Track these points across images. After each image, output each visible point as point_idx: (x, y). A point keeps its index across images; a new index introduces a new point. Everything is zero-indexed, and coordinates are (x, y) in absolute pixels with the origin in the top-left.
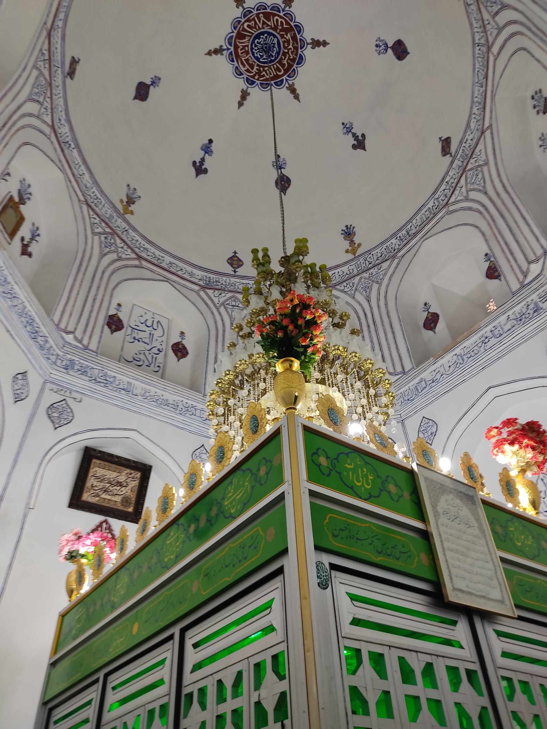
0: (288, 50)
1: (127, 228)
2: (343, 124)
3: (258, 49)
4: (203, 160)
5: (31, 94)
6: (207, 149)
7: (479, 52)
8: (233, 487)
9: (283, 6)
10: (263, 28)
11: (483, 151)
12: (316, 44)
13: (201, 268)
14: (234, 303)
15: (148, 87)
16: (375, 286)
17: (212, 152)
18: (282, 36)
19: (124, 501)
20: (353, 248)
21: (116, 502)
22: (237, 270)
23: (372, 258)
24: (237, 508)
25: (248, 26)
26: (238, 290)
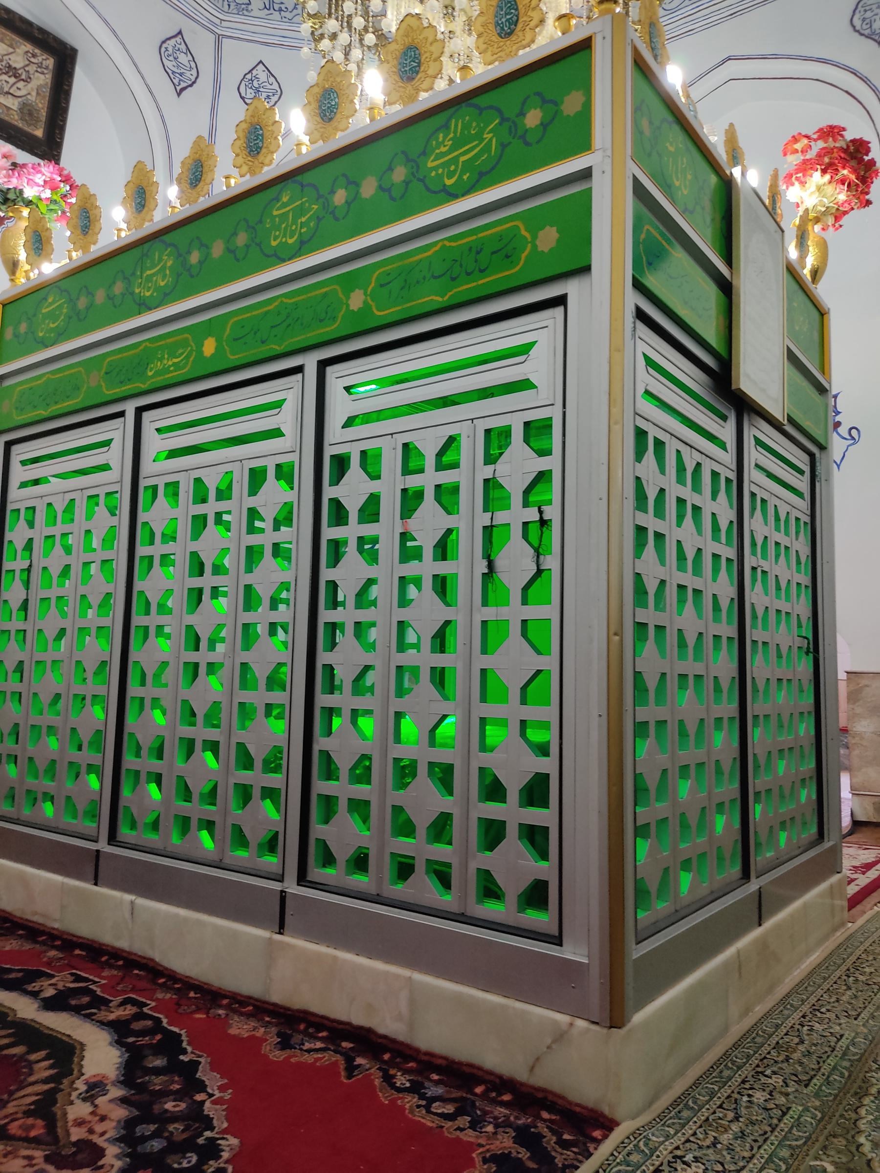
8: (452, 135)
19: (26, 111)
21: (8, 108)
24: (460, 177)
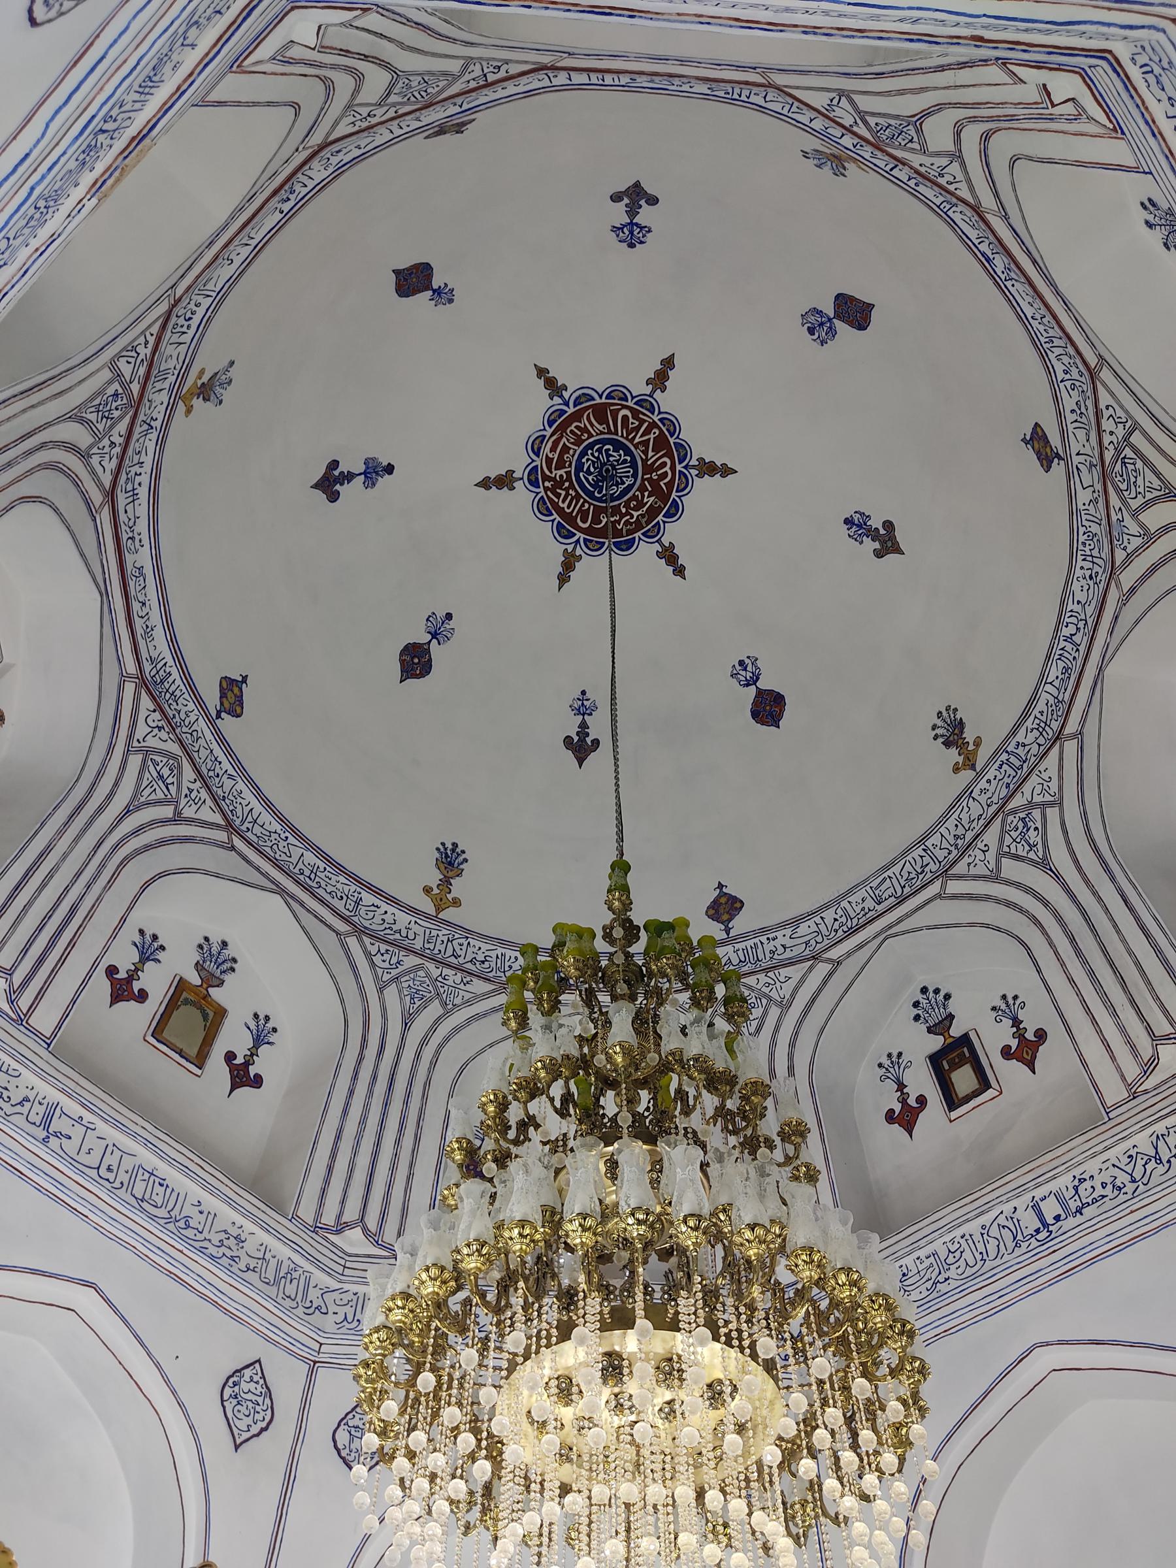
0: (627, 513)
1: (157, 424)
2: (584, 693)
3: (598, 458)
4: (349, 477)
5: (408, 74)
6: (375, 471)
7: (918, 859)
9: (694, 462)
10: (636, 447)
11: (792, 984)
12: (669, 556)
13: (173, 641)
14: (166, 772)
15: (427, 286)
16: (435, 1009)
17: (374, 484)
18: (642, 489)
20: (442, 897)
22: (223, 715)
23: (464, 948)
25: (625, 417)
26: (196, 755)
